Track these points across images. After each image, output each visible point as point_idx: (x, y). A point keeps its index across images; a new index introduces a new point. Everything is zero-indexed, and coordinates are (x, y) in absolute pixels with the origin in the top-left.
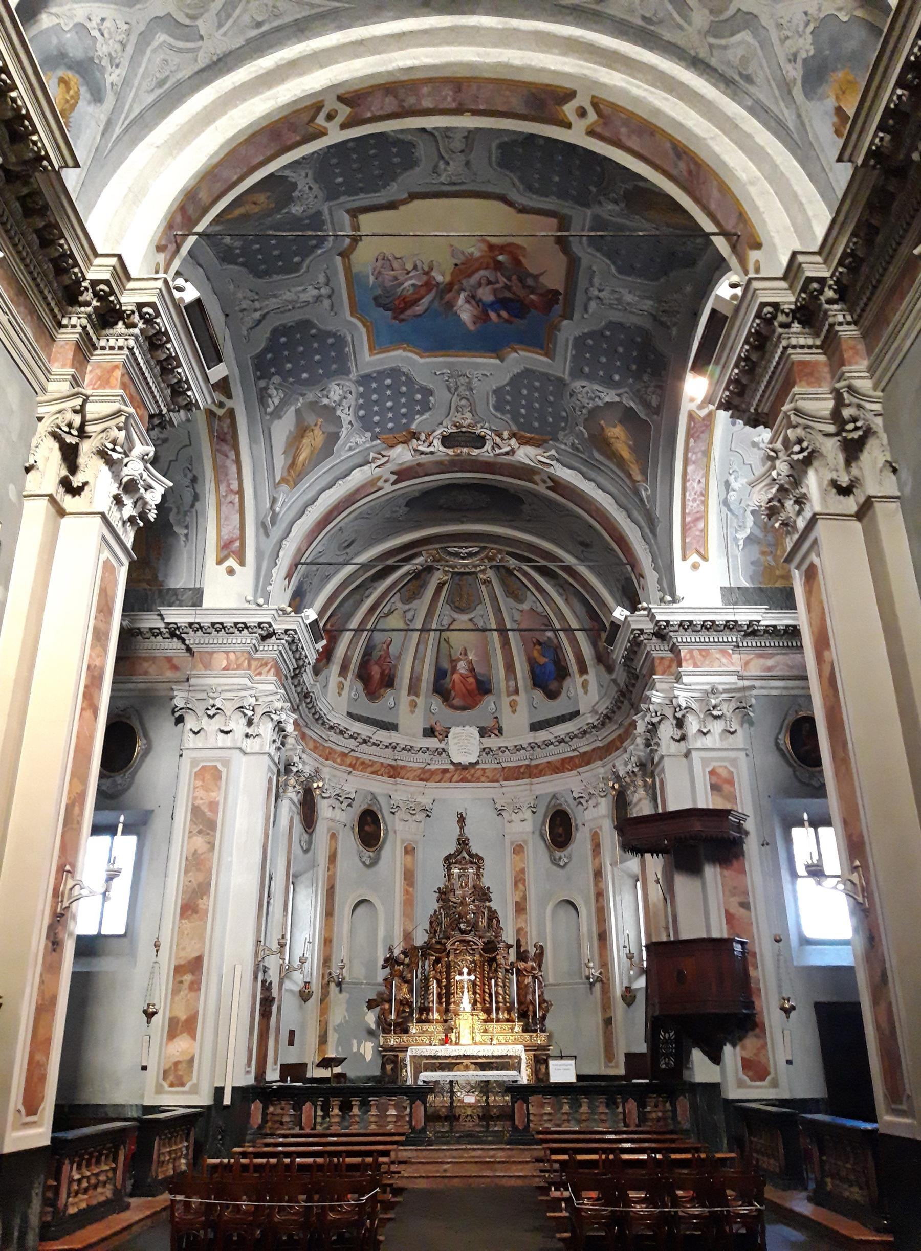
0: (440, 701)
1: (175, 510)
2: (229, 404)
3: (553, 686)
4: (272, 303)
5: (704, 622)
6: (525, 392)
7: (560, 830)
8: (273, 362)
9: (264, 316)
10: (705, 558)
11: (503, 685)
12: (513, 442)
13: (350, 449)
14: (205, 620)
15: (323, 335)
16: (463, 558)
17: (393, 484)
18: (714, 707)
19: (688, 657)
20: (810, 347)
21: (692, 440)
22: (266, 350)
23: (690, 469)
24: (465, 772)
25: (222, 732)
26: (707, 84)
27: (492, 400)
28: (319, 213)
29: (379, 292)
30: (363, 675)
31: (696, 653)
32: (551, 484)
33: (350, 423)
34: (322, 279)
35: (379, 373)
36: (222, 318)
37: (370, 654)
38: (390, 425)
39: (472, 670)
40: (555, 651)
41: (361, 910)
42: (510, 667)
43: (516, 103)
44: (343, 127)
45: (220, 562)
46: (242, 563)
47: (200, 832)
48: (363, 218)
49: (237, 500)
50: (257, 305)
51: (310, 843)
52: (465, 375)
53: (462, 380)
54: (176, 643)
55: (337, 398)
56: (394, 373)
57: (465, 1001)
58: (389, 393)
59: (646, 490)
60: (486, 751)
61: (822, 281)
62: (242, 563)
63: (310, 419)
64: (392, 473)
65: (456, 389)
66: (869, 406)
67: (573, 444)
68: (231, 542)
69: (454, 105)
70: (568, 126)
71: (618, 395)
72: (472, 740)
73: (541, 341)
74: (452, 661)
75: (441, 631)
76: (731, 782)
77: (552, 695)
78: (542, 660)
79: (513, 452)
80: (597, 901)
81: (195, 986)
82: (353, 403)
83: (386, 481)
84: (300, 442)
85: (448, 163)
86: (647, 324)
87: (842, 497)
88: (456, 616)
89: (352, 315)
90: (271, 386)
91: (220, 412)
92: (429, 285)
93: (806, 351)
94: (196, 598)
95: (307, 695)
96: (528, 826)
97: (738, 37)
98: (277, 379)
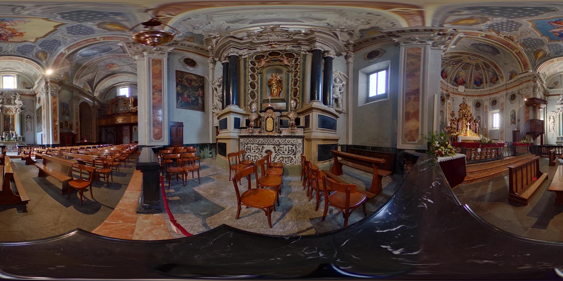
42: (470, 80)
81: (417, 100)
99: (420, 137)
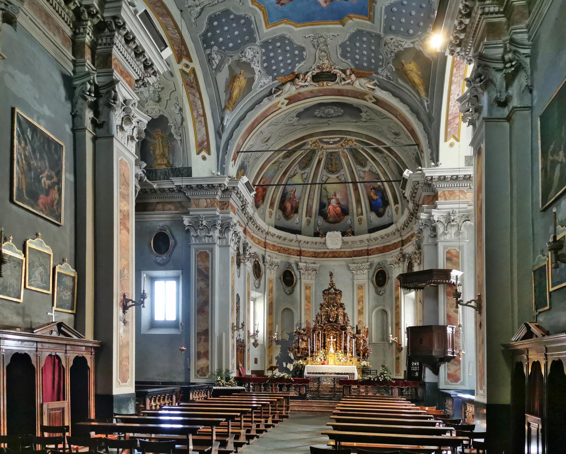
0: (322, 219)
1: (173, 127)
2: (191, 65)
5: (452, 176)
6: (358, 44)
7: (381, 279)
8: (212, 38)
9: (202, 9)
10: (458, 140)
11: (355, 211)
12: (353, 76)
13: (261, 87)
14: (194, 183)
15: (238, 18)
16: (331, 144)
17: (287, 105)
18: (453, 221)
19: (442, 195)
20: (497, 13)
21: (455, 69)
22: (207, 31)
23: (453, 87)
24: (335, 255)
25: (207, 236)
30: (282, 207)
31: (446, 193)
32: (374, 100)
33: (259, 71)
36: (179, 13)
37: (285, 197)
38: (282, 71)
39: (339, 203)
40: (382, 192)
42: (358, 201)
45: (198, 153)
46: (209, 153)
47: (202, 280)
49: (203, 120)
51: (259, 284)
52: (322, 36)
53: (322, 40)
54: (181, 195)
55: (250, 57)
56: (282, 38)
57: (332, 350)
58: (279, 51)
59: (427, 101)
60: (344, 242)
62: (209, 153)
63: (237, 71)
64: (285, 99)
65: (318, 46)
66: (522, 51)
67: (387, 76)
68: (203, 142)
71: (412, 43)
72: (338, 238)
74: (328, 199)
75: (322, 184)
77: (380, 215)
78: (375, 197)
79: (352, 84)
80: (396, 310)
81: (206, 341)
82: (260, 60)
83: (282, 104)
84: (233, 85)
87: (500, 108)
88: (329, 175)
89: (253, 3)
90: (213, 53)
91: (187, 70)
93: (494, 15)
94: (187, 172)
95: (251, 218)
96: (366, 276)
98: (215, 48)
99: (210, 373)
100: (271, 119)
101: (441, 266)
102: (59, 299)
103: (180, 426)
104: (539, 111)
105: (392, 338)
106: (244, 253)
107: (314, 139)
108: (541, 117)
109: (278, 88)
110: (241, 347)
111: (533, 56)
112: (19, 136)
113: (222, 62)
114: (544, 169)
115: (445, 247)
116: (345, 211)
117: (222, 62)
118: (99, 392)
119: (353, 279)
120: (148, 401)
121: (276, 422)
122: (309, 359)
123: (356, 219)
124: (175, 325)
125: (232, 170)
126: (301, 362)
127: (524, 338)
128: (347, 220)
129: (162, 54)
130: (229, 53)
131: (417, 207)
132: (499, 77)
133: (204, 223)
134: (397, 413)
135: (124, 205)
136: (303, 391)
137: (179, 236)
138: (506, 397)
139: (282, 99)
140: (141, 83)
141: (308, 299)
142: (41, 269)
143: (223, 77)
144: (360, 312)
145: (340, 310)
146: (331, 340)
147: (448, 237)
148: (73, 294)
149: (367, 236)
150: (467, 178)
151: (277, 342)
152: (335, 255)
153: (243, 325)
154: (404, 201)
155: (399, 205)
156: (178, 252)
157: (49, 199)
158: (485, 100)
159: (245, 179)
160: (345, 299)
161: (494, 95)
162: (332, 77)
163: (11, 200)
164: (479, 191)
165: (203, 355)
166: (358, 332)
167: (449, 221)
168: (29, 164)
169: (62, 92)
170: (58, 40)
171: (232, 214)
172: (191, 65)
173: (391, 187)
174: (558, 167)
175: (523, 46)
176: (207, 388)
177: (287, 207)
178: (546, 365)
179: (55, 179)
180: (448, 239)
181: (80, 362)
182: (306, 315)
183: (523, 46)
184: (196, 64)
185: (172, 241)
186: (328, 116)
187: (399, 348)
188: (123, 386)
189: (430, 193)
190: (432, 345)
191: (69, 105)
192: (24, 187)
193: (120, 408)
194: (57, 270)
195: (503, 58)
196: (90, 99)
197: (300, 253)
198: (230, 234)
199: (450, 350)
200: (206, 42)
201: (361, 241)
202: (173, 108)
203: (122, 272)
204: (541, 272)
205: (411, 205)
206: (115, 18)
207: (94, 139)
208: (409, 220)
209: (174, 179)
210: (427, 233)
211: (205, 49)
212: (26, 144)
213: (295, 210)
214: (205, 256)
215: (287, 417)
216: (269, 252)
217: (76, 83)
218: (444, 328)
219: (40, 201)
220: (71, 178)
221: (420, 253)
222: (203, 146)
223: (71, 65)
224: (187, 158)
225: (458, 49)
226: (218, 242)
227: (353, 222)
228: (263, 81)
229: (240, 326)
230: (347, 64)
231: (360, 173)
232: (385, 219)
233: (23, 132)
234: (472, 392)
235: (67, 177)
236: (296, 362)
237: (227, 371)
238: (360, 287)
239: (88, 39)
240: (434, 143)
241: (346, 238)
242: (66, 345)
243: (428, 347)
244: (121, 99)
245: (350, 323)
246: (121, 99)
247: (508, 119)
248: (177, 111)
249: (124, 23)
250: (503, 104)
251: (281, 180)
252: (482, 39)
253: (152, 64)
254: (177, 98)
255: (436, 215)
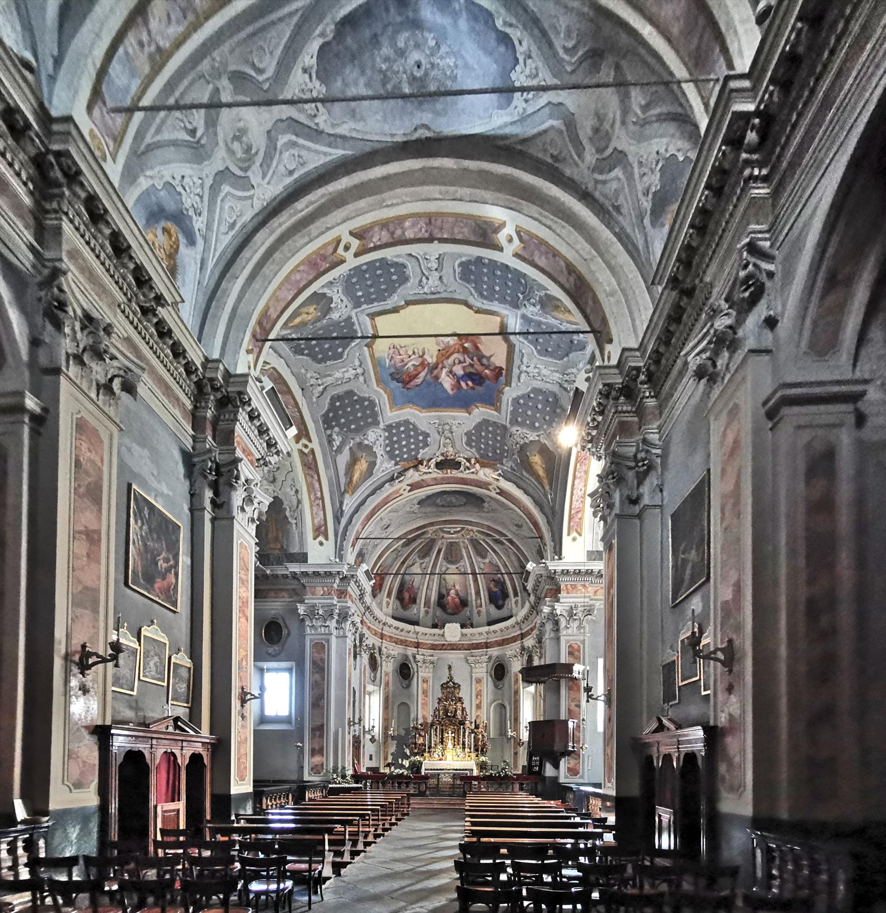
3: (500, 602)
4: (329, 380)
10: (580, 535)
12: (477, 465)
14: (311, 570)
15: (362, 400)
23: (576, 482)
24: (453, 647)
26: (590, 213)
27: (465, 439)
28: (350, 318)
29: (393, 370)
30: (400, 597)
34: (357, 363)
35: (397, 423)
39: (457, 594)
40: (501, 584)
41: (402, 708)
42: (478, 593)
43: (466, 232)
44: (356, 255)
45: (315, 539)
46: (327, 539)
48: (379, 320)
50: (320, 382)
51: (375, 677)
53: (447, 427)
54: (295, 582)
56: (407, 423)
57: (450, 745)
60: (462, 635)
61: (638, 369)
62: (327, 539)
63: (359, 454)
66: (654, 451)
68: (320, 527)
69: (427, 235)
70: (501, 249)
73: (493, 401)
76: (579, 651)
77: (499, 607)
78: (495, 590)
81: (321, 736)
85: (427, 279)
86: (556, 389)
91: (306, 451)
92: (423, 364)
94: (303, 558)
96: (484, 670)
97: (613, 174)
98: (336, 429)
100: (392, 508)
101: (563, 660)
102: (175, 690)
103: (293, 825)
104: (670, 510)
105: (510, 733)
106: (361, 645)
107: (434, 528)
108: (672, 516)
109: (401, 474)
110: (357, 743)
111: (664, 456)
112: (135, 515)
113: (343, 444)
114: (675, 566)
115: (567, 641)
116: (464, 603)
117: (343, 444)
118: (216, 792)
119: (471, 672)
120: (264, 800)
121: (400, 820)
122: (426, 755)
123: (475, 611)
124: (287, 720)
125: (351, 557)
126: (418, 758)
127: (656, 731)
128: (466, 612)
129: (287, 432)
130: (351, 435)
131: (539, 600)
132: (631, 474)
133: (321, 612)
134: (515, 808)
135: (243, 591)
136: (423, 787)
137: (293, 626)
138: (635, 789)
139: (404, 485)
140: (262, 462)
141: (425, 692)
142: (156, 659)
143: (343, 459)
144: (479, 707)
145: (459, 704)
146: (449, 735)
147: (570, 631)
148: (188, 686)
149: (486, 628)
150: (600, 575)
151: (393, 738)
152: (453, 647)
153: (360, 720)
154: (525, 594)
155: (519, 598)
156: (292, 642)
157: (165, 583)
158: (617, 496)
159: (365, 567)
160: (463, 693)
161: (626, 492)
162: (457, 465)
163: (126, 584)
164: (610, 586)
165: (317, 751)
166: (477, 727)
167: (571, 614)
168: (145, 545)
169: (181, 469)
170: (177, 413)
171: (350, 604)
172: (310, 446)
173: (512, 580)
174: (690, 565)
175: (655, 446)
176: (322, 786)
177: (406, 597)
178: (678, 759)
179: (172, 562)
180: (569, 634)
181: (196, 758)
182: (424, 709)
183: (655, 446)
184: (315, 445)
185: (285, 632)
186: (451, 505)
187: (518, 743)
188: (241, 785)
189: (552, 586)
190: (553, 741)
191: (188, 483)
192: (140, 569)
193: (238, 808)
194: (173, 660)
195: (635, 456)
196: (210, 478)
197: (418, 645)
198: (348, 625)
199: (571, 744)
200: (328, 422)
201: (479, 634)
202: (288, 490)
203: (240, 663)
204: (670, 668)
205: (532, 598)
206: (240, 393)
207: (213, 520)
208: (530, 612)
209: (288, 565)
210: (549, 627)
211: (326, 429)
212: (143, 524)
213: (413, 600)
214: (321, 647)
215: (407, 814)
216: (385, 644)
217: (195, 460)
218: (565, 722)
219: (156, 586)
220: (188, 561)
221: (541, 647)
222: (320, 531)
223: (191, 440)
224: (302, 543)
225: (590, 445)
226: (335, 632)
227: (471, 614)
228: (385, 466)
229: (357, 721)
230: (472, 453)
231: (480, 564)
232: (504, 612)
233: (140, 511)
234: (598, 785)
235: (184, 560)
236: (413, 758)
237: (344, 768)
238: (479, 681)
239: (209, 414)
240: (557, 535)
241: (465, 631)
242: (182, 741)
243: (550, 740)
244: (243, 479)
245: (468, 718)
246: (243, 479)
247: (639, 516)
248: (293, 493)
249: (250, 399)
250: (635, 502)
251: (399, 569)
252: (614, 437)
253: (276, 443)
254: (293, 480)
255: (559, 609)
